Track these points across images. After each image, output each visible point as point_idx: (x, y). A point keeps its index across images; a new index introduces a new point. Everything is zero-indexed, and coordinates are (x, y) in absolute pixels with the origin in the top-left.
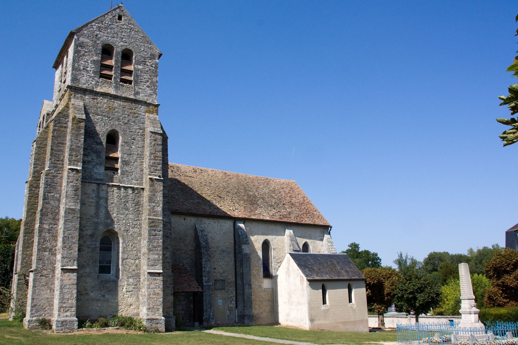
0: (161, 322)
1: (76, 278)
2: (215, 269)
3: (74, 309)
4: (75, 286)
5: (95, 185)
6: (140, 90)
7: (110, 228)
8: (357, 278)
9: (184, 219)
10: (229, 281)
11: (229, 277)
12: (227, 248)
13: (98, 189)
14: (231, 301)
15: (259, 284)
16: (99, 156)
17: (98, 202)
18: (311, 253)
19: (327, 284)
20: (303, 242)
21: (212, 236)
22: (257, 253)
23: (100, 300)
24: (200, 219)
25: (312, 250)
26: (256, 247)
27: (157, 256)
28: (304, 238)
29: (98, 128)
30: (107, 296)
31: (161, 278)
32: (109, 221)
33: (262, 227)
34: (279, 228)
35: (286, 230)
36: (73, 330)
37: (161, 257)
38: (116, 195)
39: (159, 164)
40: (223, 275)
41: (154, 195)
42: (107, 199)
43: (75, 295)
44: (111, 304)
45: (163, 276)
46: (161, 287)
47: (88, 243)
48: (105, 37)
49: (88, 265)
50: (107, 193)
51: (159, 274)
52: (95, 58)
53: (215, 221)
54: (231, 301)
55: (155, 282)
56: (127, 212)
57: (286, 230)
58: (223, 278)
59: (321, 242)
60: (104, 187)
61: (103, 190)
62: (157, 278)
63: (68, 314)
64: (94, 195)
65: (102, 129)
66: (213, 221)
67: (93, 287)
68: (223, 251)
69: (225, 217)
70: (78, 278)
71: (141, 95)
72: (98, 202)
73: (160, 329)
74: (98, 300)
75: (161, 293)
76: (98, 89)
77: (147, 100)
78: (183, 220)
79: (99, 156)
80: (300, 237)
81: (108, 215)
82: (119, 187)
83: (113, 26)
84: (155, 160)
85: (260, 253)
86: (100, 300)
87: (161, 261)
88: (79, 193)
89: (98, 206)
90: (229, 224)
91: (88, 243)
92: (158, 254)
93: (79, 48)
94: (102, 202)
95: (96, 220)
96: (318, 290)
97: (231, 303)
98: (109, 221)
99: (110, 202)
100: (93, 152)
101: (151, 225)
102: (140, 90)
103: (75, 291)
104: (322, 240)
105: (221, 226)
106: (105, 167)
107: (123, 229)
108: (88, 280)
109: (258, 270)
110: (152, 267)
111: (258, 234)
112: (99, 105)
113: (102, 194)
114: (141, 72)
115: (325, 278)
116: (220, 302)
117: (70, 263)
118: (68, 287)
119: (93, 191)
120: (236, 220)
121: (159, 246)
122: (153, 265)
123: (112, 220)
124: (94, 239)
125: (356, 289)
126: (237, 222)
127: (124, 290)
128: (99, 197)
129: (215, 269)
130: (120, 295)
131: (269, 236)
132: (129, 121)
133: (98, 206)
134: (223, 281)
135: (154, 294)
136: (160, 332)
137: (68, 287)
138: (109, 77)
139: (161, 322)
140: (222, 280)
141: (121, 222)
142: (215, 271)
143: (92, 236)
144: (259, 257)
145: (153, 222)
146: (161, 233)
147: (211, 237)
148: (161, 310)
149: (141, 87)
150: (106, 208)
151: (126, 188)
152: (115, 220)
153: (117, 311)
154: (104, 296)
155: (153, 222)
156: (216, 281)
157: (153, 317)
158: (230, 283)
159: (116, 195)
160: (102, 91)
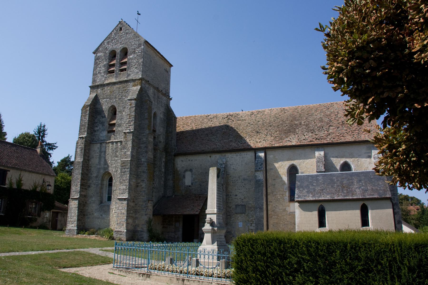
0: (123, 233)
1: (77, 203)
2: (236, 195)
3: (76, 222)
4: (77, 209)
5: (99, 144)
6: (131, 73)
7: (107, 170)
8: (376, 196)
9: (210, 157)
10: (250, 206)
11: (251, 202)
12: (249, 176)
13: (101, 147)
14: (251, 224)
15: (284, 208)
16: (103, 125)
17: (100, 155)
18: (353, 171)
19: (325, 205)
20: (342, 162)
21: (234, 167)
22: (281, 178)
23: (100, 218)
24: (223, 155)
25: (354, 169)
26: (280, 173)
27: (125, 187)
28: (342, 157)
29: (104, 107)
30: (103, 216)
31: (126, 202)
32: (106, 166)
33: (287, 153)
34: (308, 150)
35: (316, 152)
36: (74, 235)
37: (128, 187)
38: (110, 148)
39: (132, 121)
40: (244, 201)
41: (126, 144)
42: (105, 152)
43: (77, 214)
44: (105, 221)
45: (128, 201)
46: (126, 208)
47: (94, 182)
48: (110, 47)
49: (94, 195)
50: (106, 148)
51: (125, 199)
52: (105, 63)
53: (237, 154)
54: (251, 224)
55: (122, 205)
56: (116, 159)
57: (316, 152)
58: (243, 204)
59: (368, 160)
60: (104, 145)
61: (103, 147)
62: (123, 202)
63: (73, 225)
64: (98, 151)
65: (105, 106)
66: (235, 155)
67: (96, 210)
68: (244, 180)
69: (250, 149)
70: (79, 204)
71: (131, 75)
72: (100, 155)
73: (122, 239)
74: (99, 218)
75: (125, 213)
76: (106, 82)
77: (135, 77)
78: (209, 158)
79: (103, 125)
80: (337, 157)
81: (106, 163)
82: (112, 143)
83: (116, 37)
84: (130, 118)
85: (285, 178)
86: (100, 218)
87: (127, 190)
88: (83, 151)
89: (100, 158)
90: (250, 155)
91: (94, 182)
92: (126, 185)
93: (97, 61)
94: (103, 154)
95: (99, 167)
96: (311, 211)
97: (251, 226)
98: (106, 166)
99: (107, 153)
100: (100, 124)
101: (123, 165)
102: (131, 73)
103: (77, 212)
104: (370, 157)
105: (243, 158)
106: (108, 131)
107: (114, 170)
108: (94, 205)
109: (283, 195)
110: (122, 195)
111: (282, 161)
112: (105, 92)
113: (103, 149)
114: (132, 60)
115: (327, 199)
116: (240, 225)
117: (76, 195)
118: (73, 209)
119: (98, 148)
120: (256, 150)
121: (127, 179)
122: (122, 194)
123: (108, 165)
124: (97, 179)
125: (374, 211)
126: (257, 153)
127: (114, 211)
128: (101, 152)
129: (236, 195)
130: (111, 215)
131: (296, 161)
132: (122, 96)
133: (100, 158)
134: (244, 206)
135: (121, 214)
136: (122, 241)
137: (73, 209)
138: (113, 72)
139: (123, 233)
140: (242, 205)
141: (113, 165)
142: (236, 197)
143: (97, 177)
144: (284, 182)
145: (124, 163)
146: (129, 170)
147: (233, 169)
148: (125, 225)
149: (132, 70)
150: (105, 158)
151: (117, 142)
152: (110, 165)
153: (109, 226)
154: (102, 215)
155: (124, 163)
156: (237, 206)
157: (120, 230)
158: (251, 208)
159: (110, 148)
160: (108, 82)
